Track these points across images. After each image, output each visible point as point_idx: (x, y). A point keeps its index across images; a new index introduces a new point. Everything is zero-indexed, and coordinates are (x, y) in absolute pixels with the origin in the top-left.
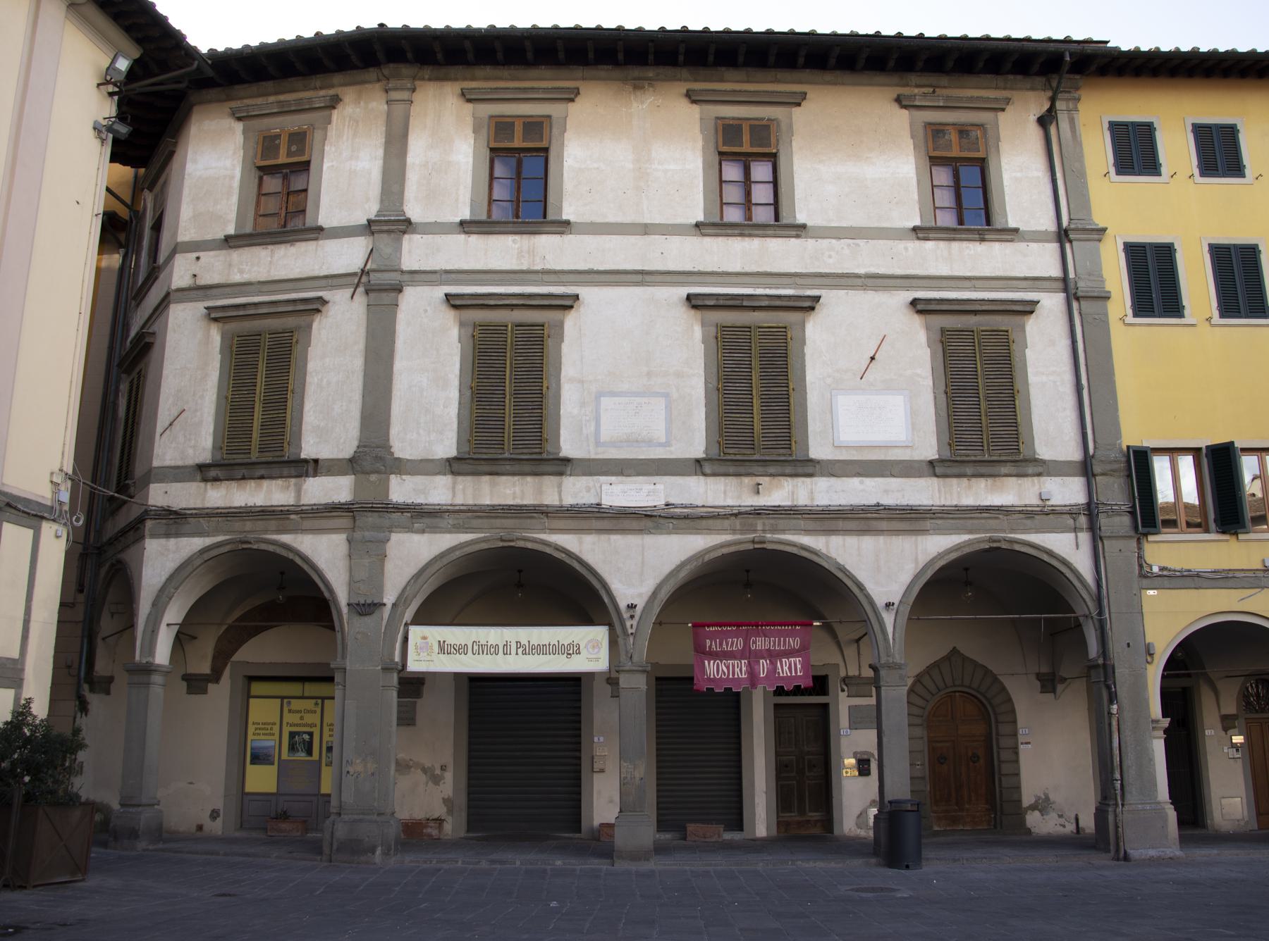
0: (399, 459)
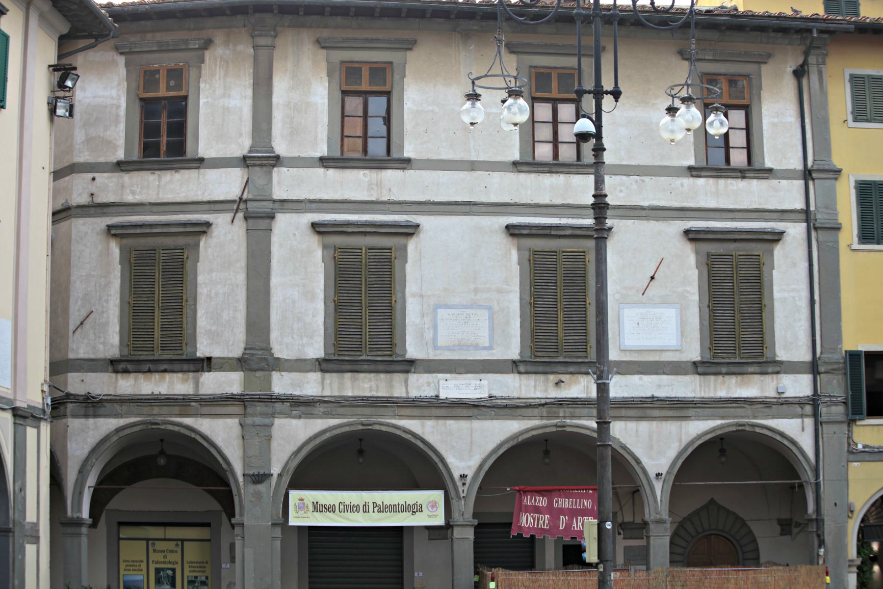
0: (278, 359)
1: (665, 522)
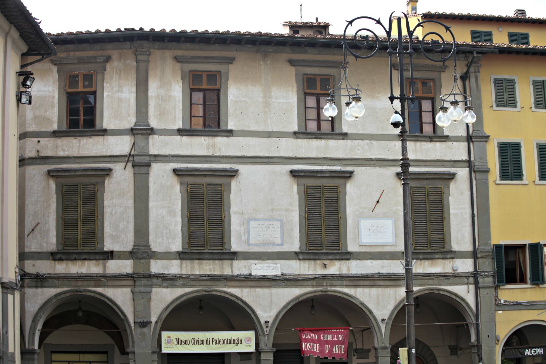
0: (154, 252)
1: (387, 348)
